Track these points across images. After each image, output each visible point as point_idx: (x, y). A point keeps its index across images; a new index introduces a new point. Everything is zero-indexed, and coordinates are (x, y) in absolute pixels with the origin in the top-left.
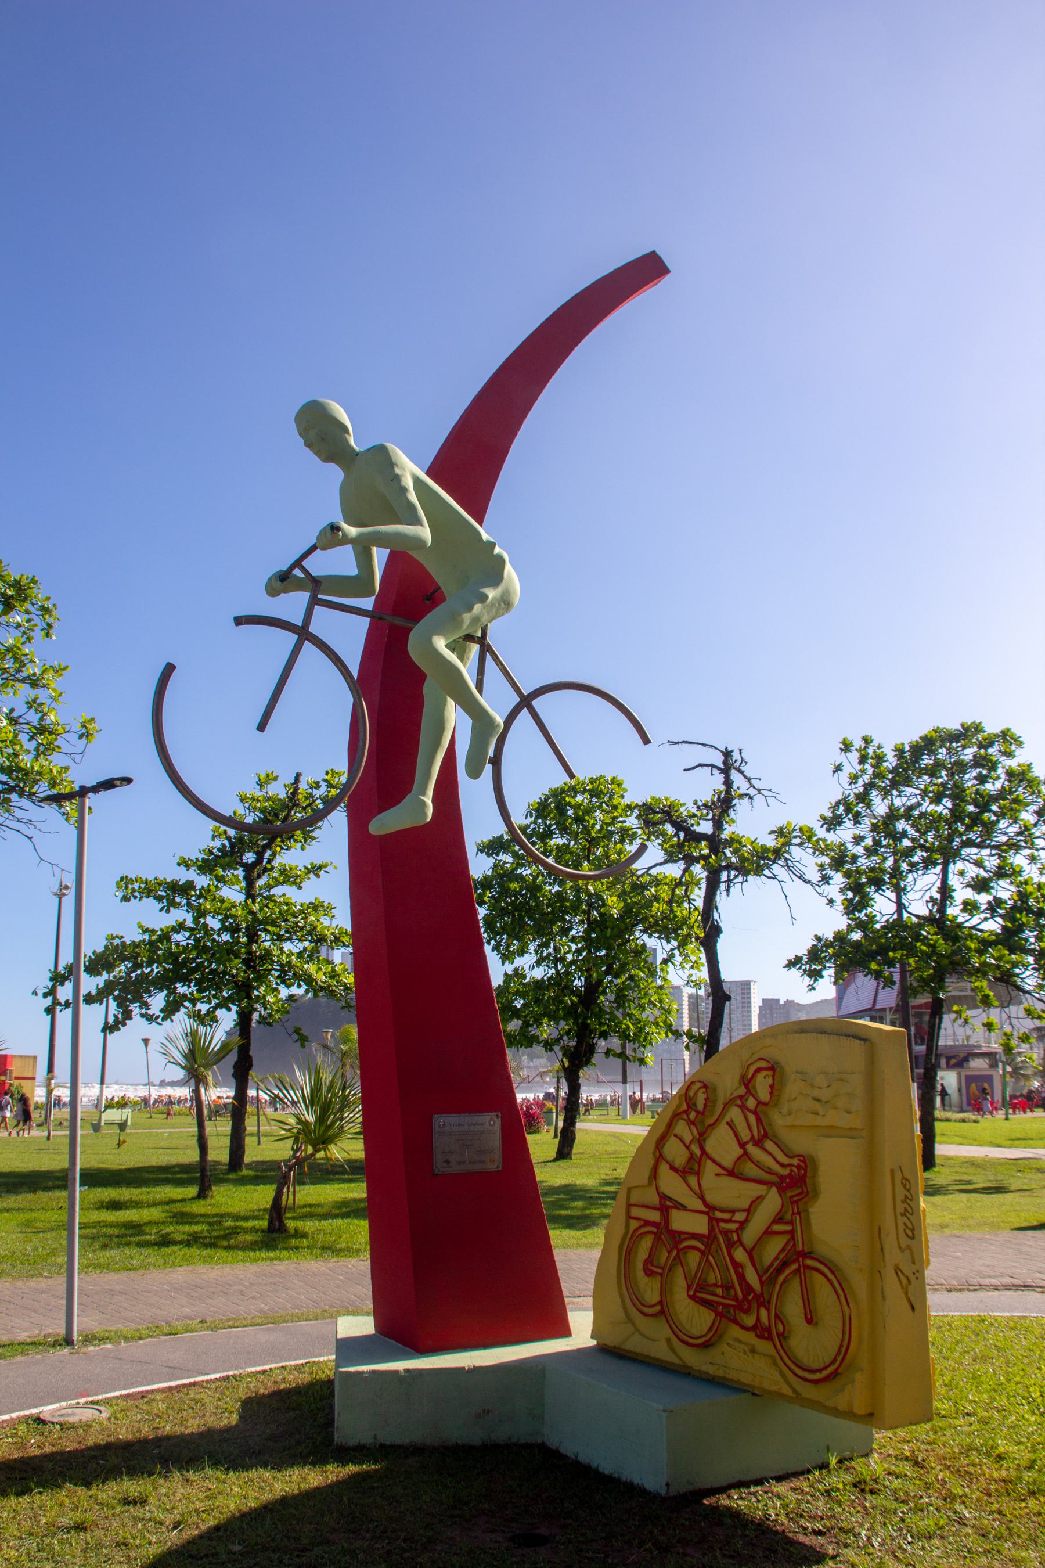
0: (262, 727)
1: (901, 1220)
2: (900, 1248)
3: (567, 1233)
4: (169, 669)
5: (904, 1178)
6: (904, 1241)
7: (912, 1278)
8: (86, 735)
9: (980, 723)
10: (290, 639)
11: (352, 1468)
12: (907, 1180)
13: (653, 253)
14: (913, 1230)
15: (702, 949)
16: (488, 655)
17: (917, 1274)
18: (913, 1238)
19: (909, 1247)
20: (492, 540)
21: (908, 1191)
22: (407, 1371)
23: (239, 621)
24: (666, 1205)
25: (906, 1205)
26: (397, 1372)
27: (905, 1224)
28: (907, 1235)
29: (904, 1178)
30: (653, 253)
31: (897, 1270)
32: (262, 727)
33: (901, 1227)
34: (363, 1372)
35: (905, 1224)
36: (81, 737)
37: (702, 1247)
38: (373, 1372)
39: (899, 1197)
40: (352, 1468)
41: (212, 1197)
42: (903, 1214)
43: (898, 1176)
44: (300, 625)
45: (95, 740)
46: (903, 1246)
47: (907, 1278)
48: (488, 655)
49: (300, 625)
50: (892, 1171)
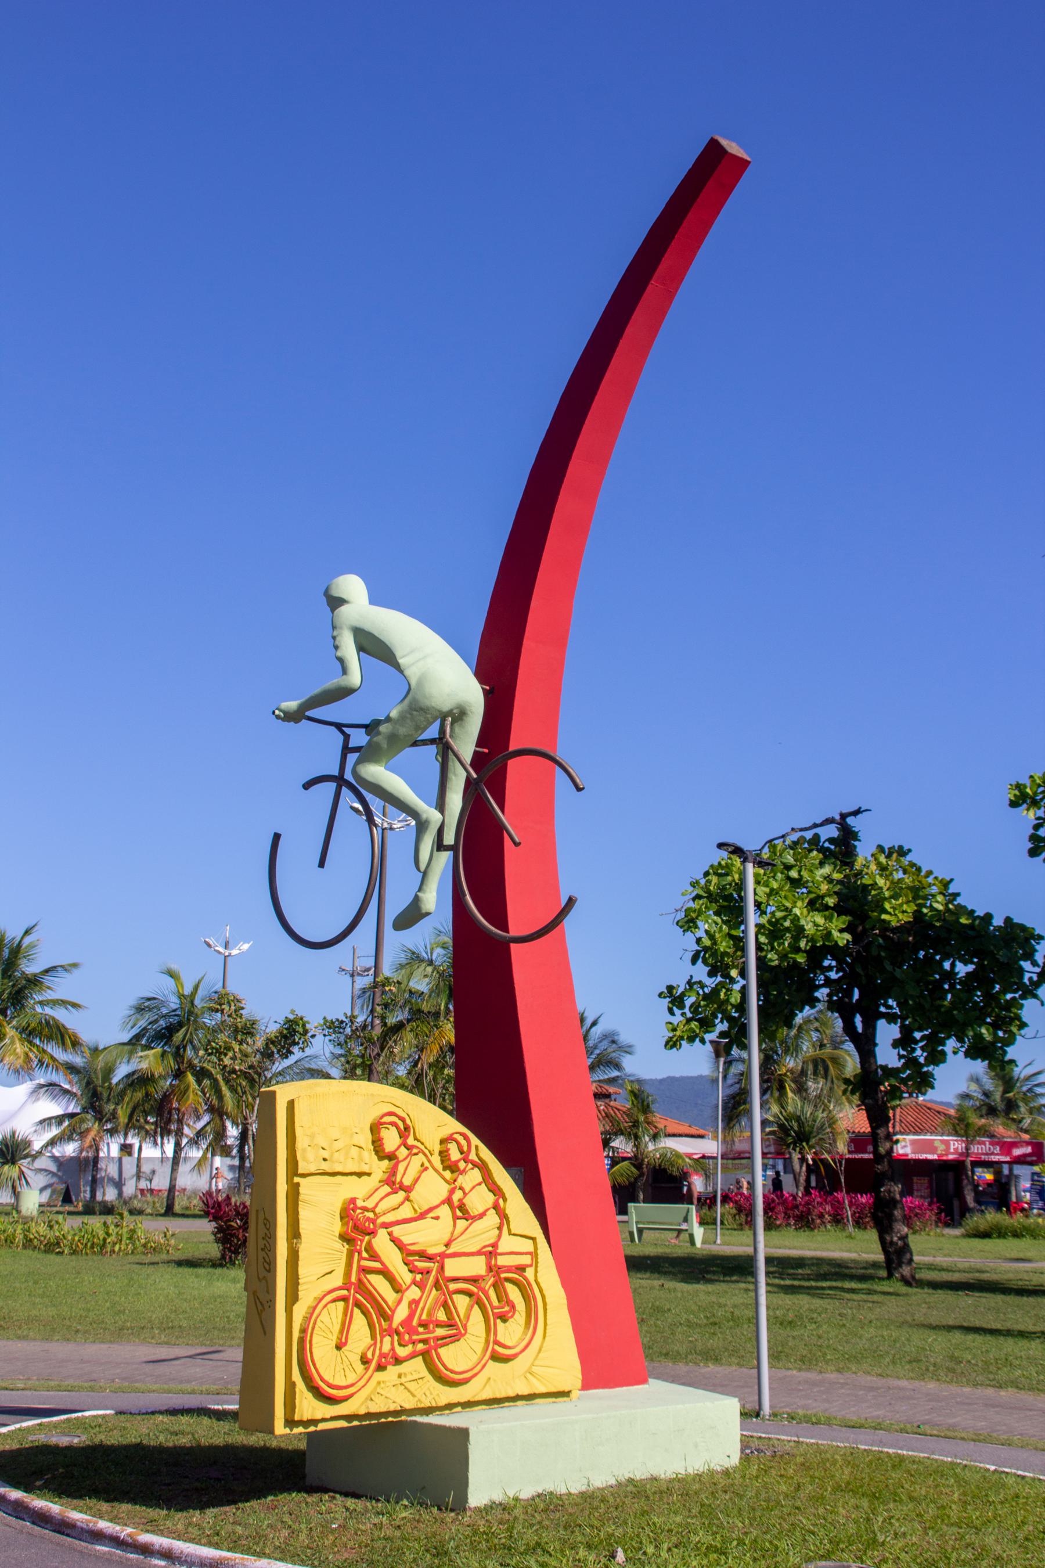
0: (322, 864)
1: (262, 1254)
2: (267, 1282)
3: (443, 1348)
4: (277, 837)
5: (265, 1219)
6: (263, 1273)
10: (333, 786)
14: (269, 1264)
15: (898, 925)
16: (344, 729)
20: (749, 159)
21: (268, 1229)
23: (307, 786)
24: (905, 1461)
25: (265, 1242)
28: (265, 1268)
29: (265, 1219)
32: (322, 864)
33: (261, 1260)
37: (433, 1351)
39: (261, 1234)
42: (262, 1250)
44: (337, 774)
46: (261, 1277)
48: (344, 729)
49: (337, 774)
50: (257, 1211)
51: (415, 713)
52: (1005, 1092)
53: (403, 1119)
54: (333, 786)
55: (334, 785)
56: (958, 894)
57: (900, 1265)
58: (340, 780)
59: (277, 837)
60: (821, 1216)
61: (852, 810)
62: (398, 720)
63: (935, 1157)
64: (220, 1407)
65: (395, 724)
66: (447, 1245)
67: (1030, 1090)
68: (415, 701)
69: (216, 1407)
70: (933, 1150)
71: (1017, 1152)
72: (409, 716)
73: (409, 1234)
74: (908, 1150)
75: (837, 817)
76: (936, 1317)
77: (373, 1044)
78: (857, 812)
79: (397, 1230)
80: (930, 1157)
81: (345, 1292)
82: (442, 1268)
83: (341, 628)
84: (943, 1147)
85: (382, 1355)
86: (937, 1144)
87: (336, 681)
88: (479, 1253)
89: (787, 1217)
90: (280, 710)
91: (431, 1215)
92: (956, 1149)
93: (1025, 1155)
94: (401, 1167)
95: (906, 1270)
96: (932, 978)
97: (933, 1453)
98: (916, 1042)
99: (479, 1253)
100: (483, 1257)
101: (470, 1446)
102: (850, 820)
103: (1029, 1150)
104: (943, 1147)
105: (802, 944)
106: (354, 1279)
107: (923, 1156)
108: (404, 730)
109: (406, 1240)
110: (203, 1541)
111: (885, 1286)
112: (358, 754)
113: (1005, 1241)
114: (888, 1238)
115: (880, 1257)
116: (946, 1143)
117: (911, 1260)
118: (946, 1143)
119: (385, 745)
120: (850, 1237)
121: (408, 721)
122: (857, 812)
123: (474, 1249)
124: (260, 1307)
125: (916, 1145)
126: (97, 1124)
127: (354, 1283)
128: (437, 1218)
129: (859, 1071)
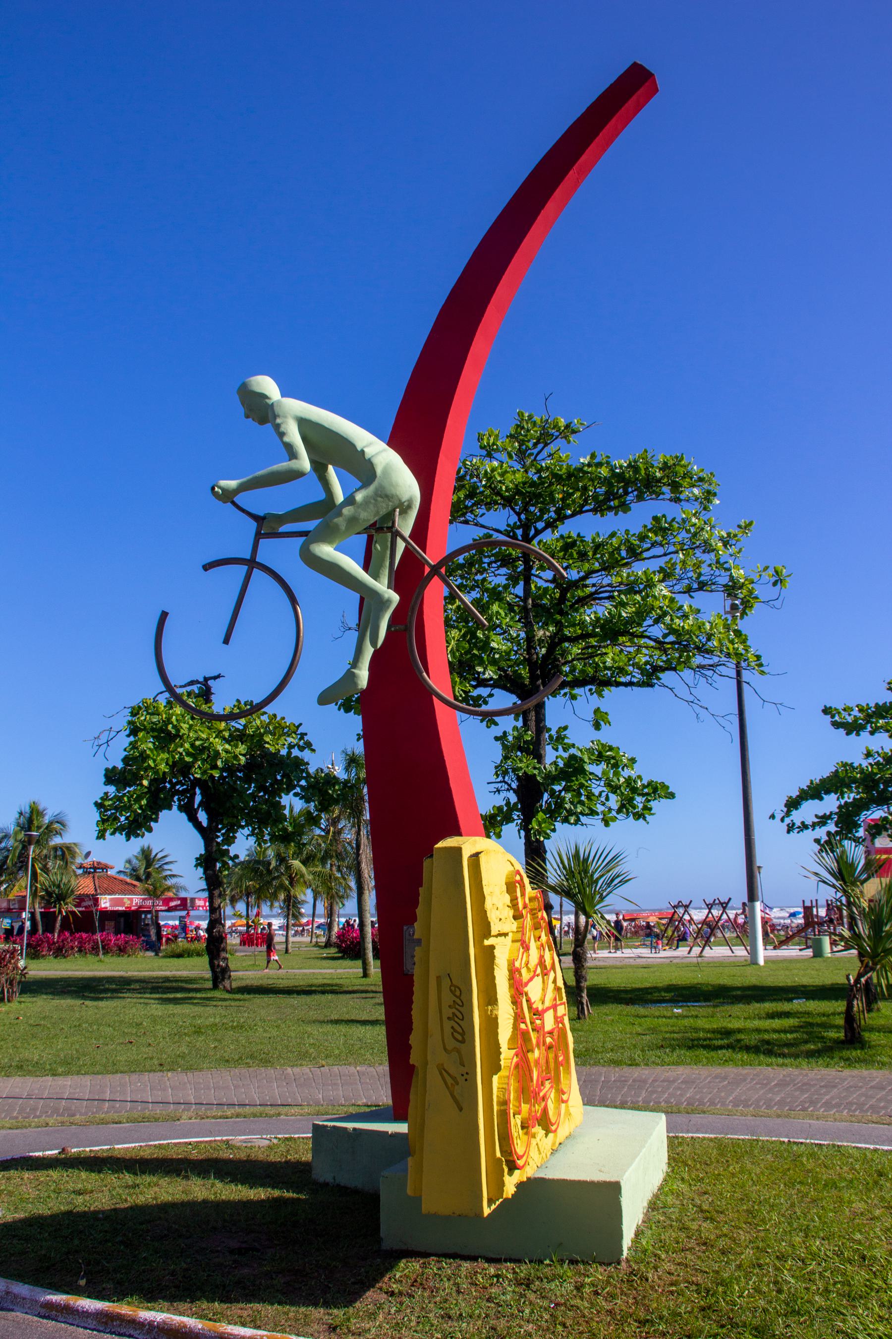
0: (226, 641)
2: (445, 1049)
4: (164, 615)
6: (451, 1044)
7: (461, 1080)
8: (778, 581)
9: (602, 516)
10: (244, 569)
11: (276, 1193)
12: (456, 987)
13: (635, 65)
14: (463, 1034)
17: (466, 1076)
18: (463, 1041)
19: (458, 1051)
21: (459, 998)
22: (355, 1129)
23: (207, 567)
25: (454, 1010)
26: (346, 1129)
27: (452, 1027)
30: (635, 65)
31: (442, 1069)
32: (226, 641)
33: (448, 1030)
34: (327, 1126)
35: (452, 1027)
36: (775, 584)
38: (334, 1127)
40: (276, 1193)
41: (878, 1010)
43: (446, 983)
45: (788, 582)
46: (449, 1048)
47: (454, 1078)
51: (379, 499)
52: (147, 868)
54: (244, 569)
55: (245, 568)
56: (306, 734)
57: (223, 980)
58: (252, 563)
59: (164, 615)
60: (72, 948)
61: (213, 675)
62: (361, 504)
63: (124, 909)
64: (40, 1154)
65: (358, 507)
67: (160, 867)
68: (381, 488)
69: (37, 1154)
70: (123, 904)
71: (172, 904)
72: (373, 501)
74: (108, 905)
75: (201, 680)
76: (313, 1015)
78: (215, 678)
80: (120, 909)
83: (285, 417)
84: (129, 902)
86: (125, 900)
87: (285, 465)
89: (50, 950)
90: (220, 487)
92: (137, 904)
93: (176, 906)
95: (227, 983)
97: (727, 1134)
98: (219, 830)
101: (622, 1199)
102: (210, 683)
103: (179, 902)
104: (129, 902)
105: (219, 763)
107: (116, 908)
108: (365, 514)
111: (217, 994)
112: (304, 538)
113: (191, 959)
114: (216, 962)
115: (208, 974)
116: (131, 900)
117: (230, 976)
118: (131, 900)
119: (343, 528)
120: (100, 961)
121: (371, 506)
122: (215, 678)
124: (450, 1081)
125: (114, 902)
129: (203, 852)
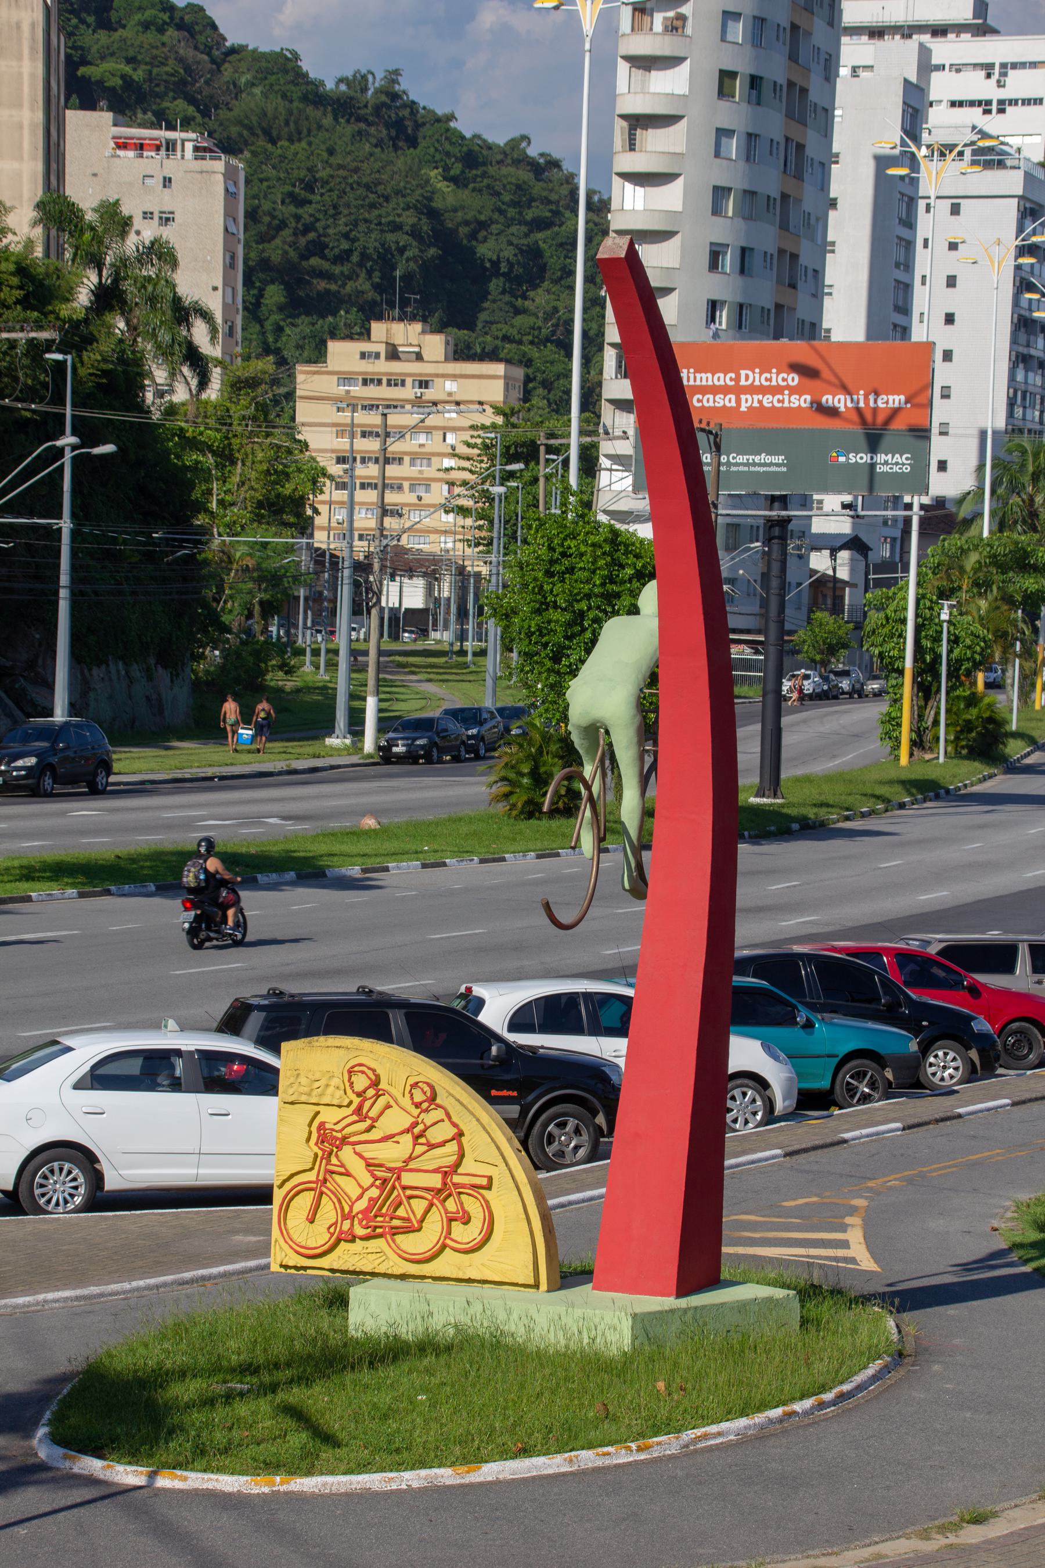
53: (374, 1071)
66: (407, 1161)
73: (373, 1152)
77: (703, 430)
79: (358, 1148)
81: (314, 1185)
82: (399, 1178)
85: (341, 1232)
88: (435, 1171)
91: (394, 1139)
94: (367, 1104)
96: (48, 1415)
99: (435, 1171)
100: (440, 1175)
106: (321, 1177)
109: (366, 1155)
110: (920, 620)
123: (431, 1168)
126: (120, 663)
127: (1019, 406)
128: (398, 1142)
